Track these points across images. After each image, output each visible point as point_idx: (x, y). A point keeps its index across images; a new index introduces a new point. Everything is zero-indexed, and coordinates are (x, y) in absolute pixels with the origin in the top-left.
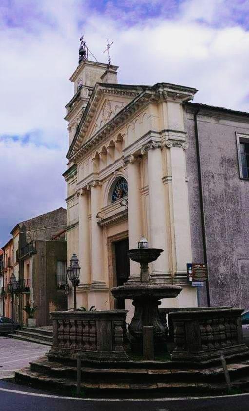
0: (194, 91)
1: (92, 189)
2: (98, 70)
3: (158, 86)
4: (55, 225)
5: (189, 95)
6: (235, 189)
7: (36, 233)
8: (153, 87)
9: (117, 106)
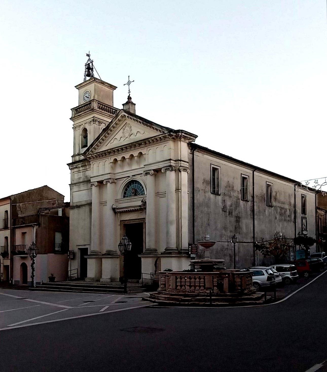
0: (196, 137)
1: (108, 184)
2: (103, 87)
3: (178, 131)
4: (40, 200)
5: (193, 139)
7: (25, 205)
8: (175, 131)
9: (138, 131)
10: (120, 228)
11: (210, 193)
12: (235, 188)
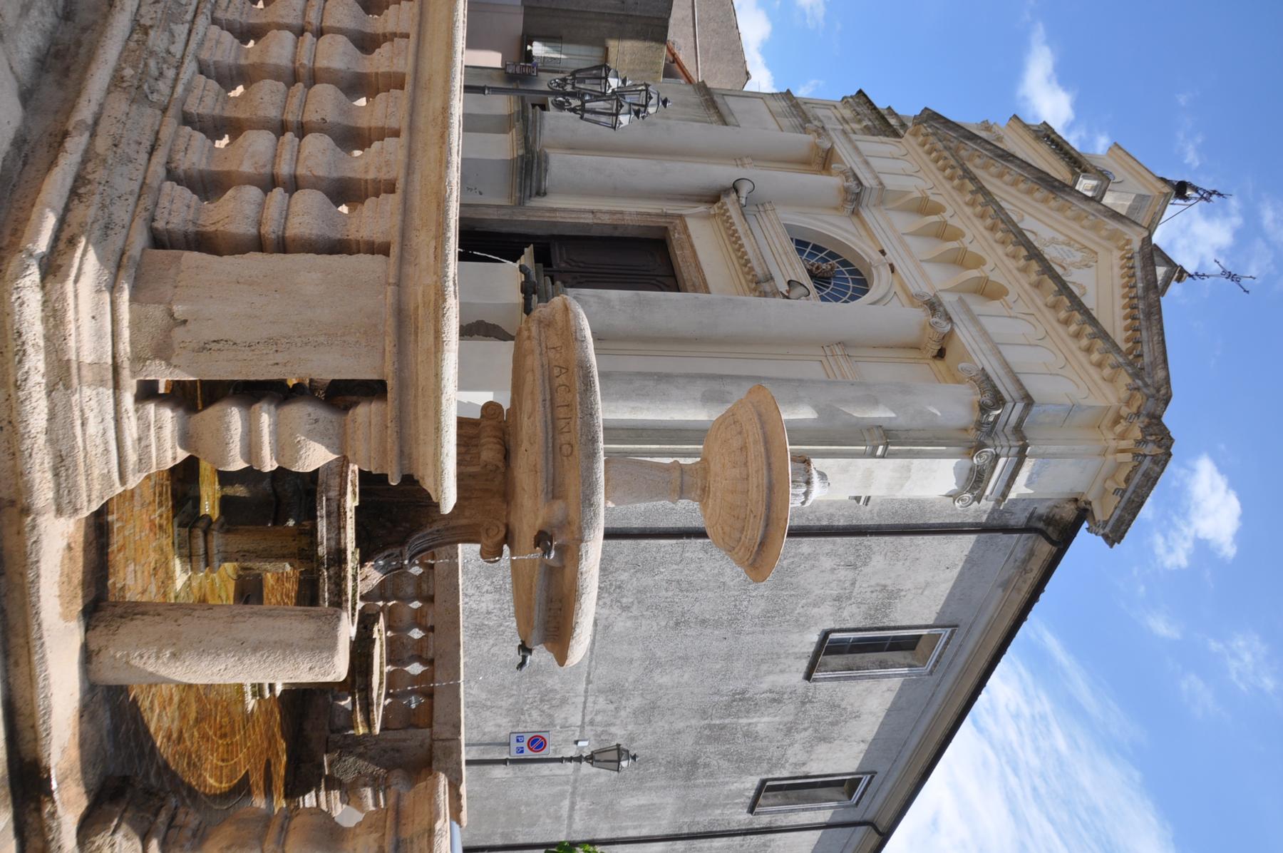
6: (802, 619)
10: (649, 214)
11: (829, 625)
12: (822, 749)
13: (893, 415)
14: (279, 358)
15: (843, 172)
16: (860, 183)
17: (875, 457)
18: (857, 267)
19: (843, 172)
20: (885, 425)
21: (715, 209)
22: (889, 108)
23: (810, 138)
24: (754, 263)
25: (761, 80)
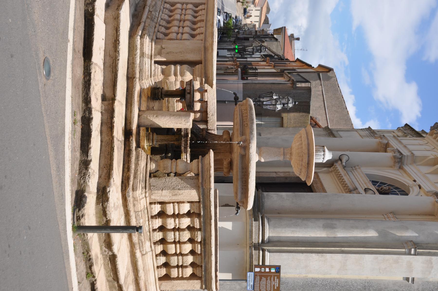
13: (417, 235)
14: (182, 55)
15: (393, 150)
16: (401, 154)
17: (411, 255)
18: (403, 189)
19: (393, 150)
20: (414, 240)
21: (332, 169)
22: (423, 130)
23: (378, 140)
24: (349, 184)
25: (357, 124)
